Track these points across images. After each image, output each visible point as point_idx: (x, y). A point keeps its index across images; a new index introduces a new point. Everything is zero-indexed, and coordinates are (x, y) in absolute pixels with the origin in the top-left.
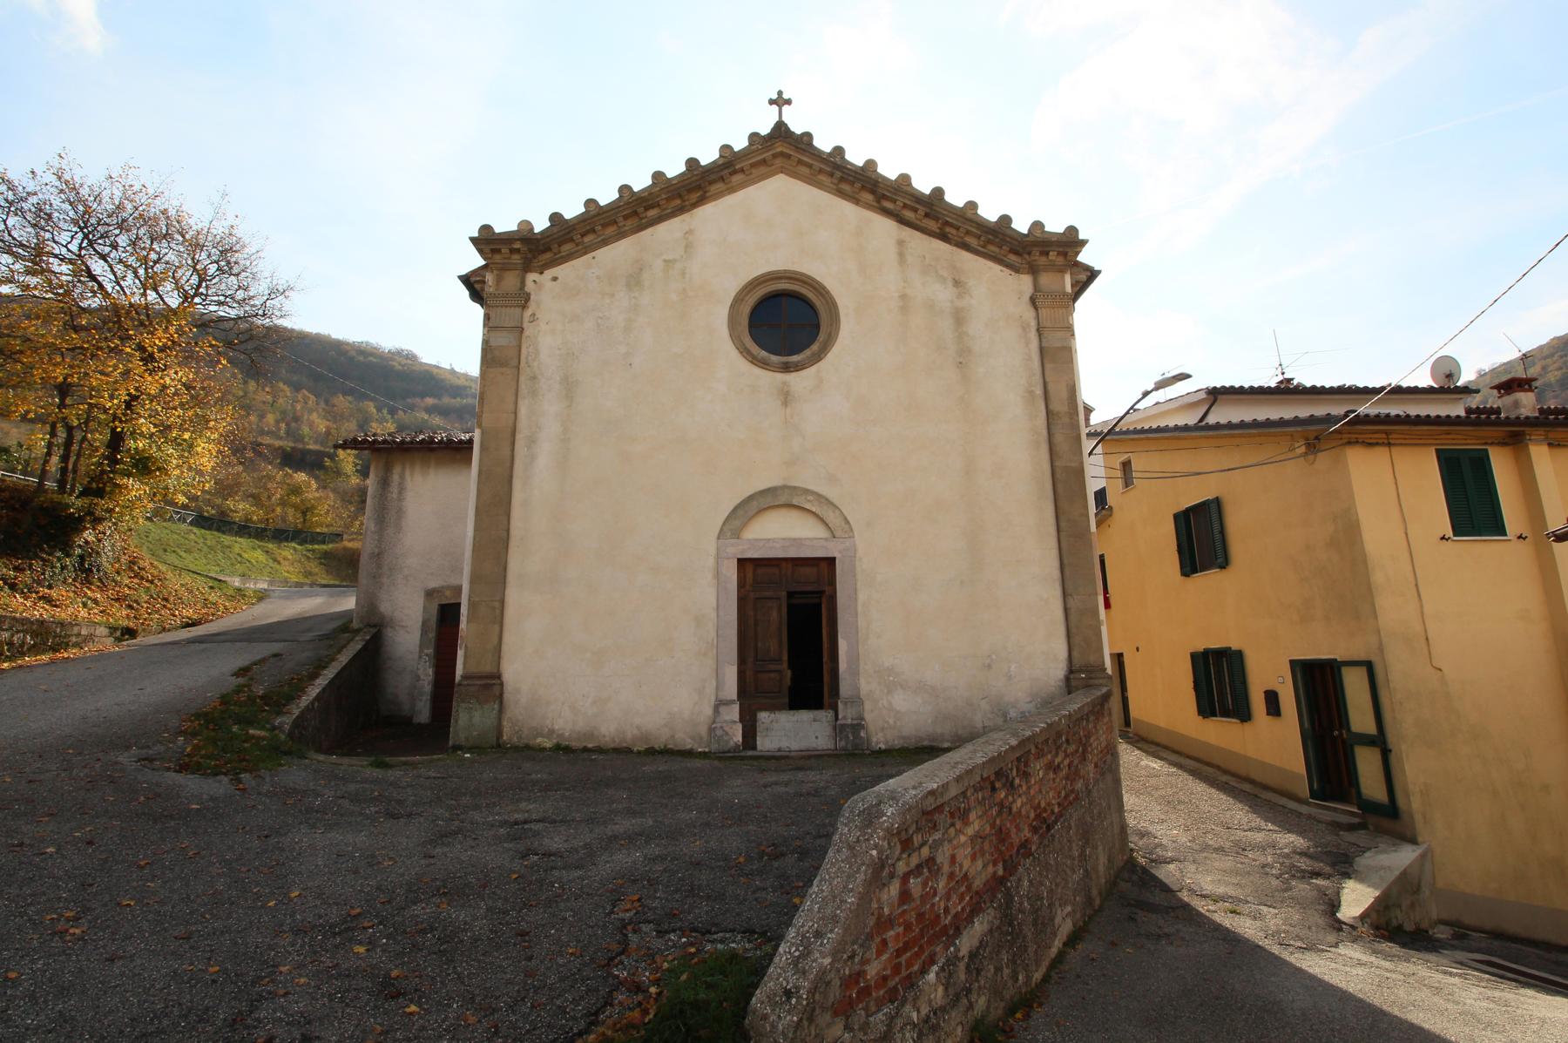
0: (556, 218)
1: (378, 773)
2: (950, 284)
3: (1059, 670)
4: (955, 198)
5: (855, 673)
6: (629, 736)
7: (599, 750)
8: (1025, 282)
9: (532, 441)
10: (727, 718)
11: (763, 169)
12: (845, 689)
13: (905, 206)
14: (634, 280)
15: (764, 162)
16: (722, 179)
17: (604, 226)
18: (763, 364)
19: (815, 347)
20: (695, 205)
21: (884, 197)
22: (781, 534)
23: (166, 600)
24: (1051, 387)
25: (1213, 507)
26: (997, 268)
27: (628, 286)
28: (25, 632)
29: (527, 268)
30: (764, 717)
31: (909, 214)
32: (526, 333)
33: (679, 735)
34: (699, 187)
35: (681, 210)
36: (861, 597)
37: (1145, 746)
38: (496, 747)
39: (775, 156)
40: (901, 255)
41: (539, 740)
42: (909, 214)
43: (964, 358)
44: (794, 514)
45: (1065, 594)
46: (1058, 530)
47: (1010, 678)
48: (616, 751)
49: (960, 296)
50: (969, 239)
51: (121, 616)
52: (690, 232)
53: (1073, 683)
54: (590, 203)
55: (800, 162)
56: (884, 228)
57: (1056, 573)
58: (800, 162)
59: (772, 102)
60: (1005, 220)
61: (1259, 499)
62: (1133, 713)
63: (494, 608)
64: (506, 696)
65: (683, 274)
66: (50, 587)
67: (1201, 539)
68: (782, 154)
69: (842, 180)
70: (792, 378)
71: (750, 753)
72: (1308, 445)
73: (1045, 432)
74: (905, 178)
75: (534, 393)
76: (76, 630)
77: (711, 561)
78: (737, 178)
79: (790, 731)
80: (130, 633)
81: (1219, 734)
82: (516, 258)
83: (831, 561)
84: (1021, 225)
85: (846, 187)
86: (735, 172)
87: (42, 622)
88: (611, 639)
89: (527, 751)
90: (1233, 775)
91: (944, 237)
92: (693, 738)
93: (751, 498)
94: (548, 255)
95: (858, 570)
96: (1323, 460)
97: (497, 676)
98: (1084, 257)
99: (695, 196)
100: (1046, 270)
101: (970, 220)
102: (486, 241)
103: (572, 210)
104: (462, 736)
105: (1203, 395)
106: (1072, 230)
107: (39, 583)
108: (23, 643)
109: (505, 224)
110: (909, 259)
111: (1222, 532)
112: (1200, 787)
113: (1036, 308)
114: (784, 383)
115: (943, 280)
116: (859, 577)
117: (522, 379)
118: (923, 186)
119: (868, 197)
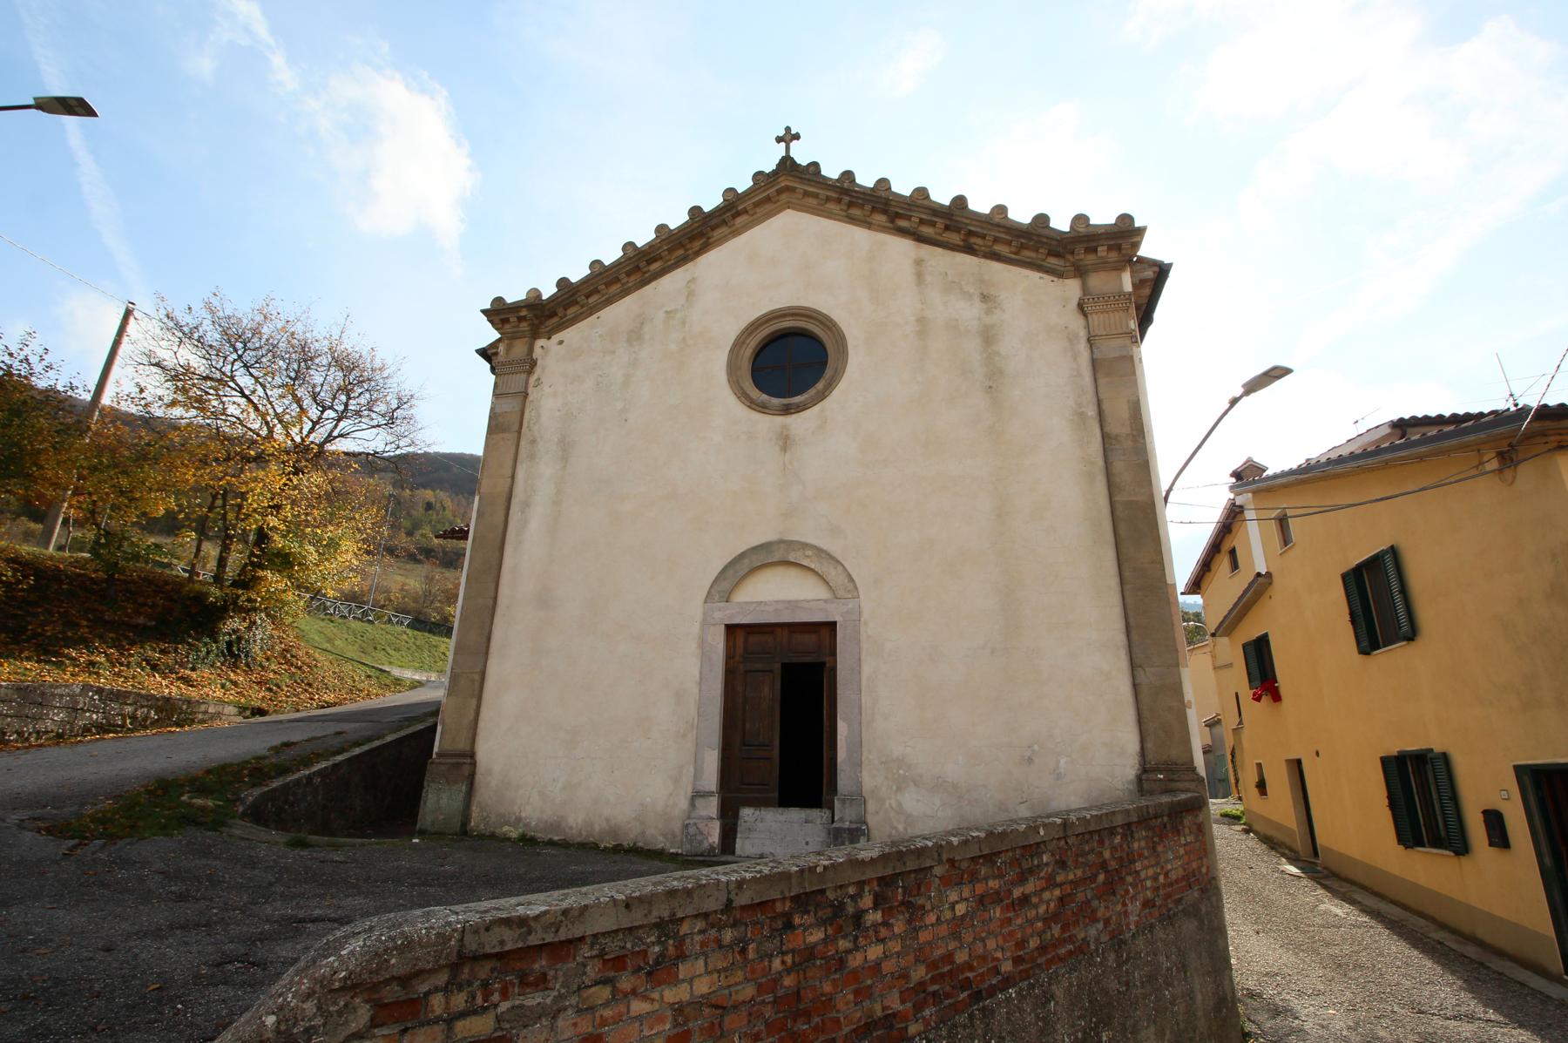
0: (563, 283)
1: (292, 856)
2: (977, 300)
3: (1128, 768)
4: (980, 205)
5: (858, 765)
6: (597, 829)
7: (565, 845)
8: (1072, 288)
9: (526, 505)
10: (704, 813)
11: (768, 207)
12: (844, 782)
13: (922, 221)
14: (635, 335)
15: (768, 199)
16: (724, 223)
17: (608, 285)
18: (762, 408)
19: (820, 385)
20: (698, 253)
21: (898, 216)
22: (777, 595)
23: (310, 685)
24: (1105, 406)
25: (1388, 559)
26: (1034, 276)
27: (629, 341)
28: (150, 707)
29: (535, 335)
30: (747, 813)
31: (927, 231)
32: (530, 398)
33: (650, 831)
34: (702, 234)
35: (685, 260)
36: (866, 670)
37: (1336, 885)
38: (462, 832)
39: (779, 192)
40: (919, 276)
41: (506, 828)
42: (927, 231)
43: (994, 379)
44: (793, 572)
45: (1133, 666)
46: (1122, 582)
47: (1058, 777)
48: (583, 846)
49: (989, 312)
50: (998, 248)
51: (257, 697)
52: (693, 280)
53: (1146, 786)
54: (595, 264)
55: (806, 194)
56: (900, 249)
57: (1120, 638)
58: (806, 194)
59: (779, 140)
60: (1042, 219)
61: (1448, 543)
62: (1319, 841)
63: (473, 681)
64: (478, 777)
65: (684, 323)
66: (193, 669)
67: (1378, 604)
68: (788, 189)
69: (850, 205)
70: (793, 421)
71: (730, 858)
72: (1501, 455)
73: (1100, 462)
74: (922, 192)
75: (532, 457)
76: (203, 707)
77: (696, 629)
78: (740, 220)
79: (780, 838)
80: (261, 712)
81: (1426, 870)
82: (524, 326)
83: (832, 626)
84: (1061, 223)
85: (855, 212)
86: (738, 214)
87: (168, 700)
88: (593, 722)
89: (492, 840)
90: (1454, 931)
91: (969, 250)
92: (665, 836)
93: (742, 556)
94: (555, 320)
95: (863, 637)
96: (1526, 474)
97: (471, 755)
98: (1147, 250)
99: (697, 244)
100: (1096, 270)
101: (998, 225)
102: (498, 313)
103: (578, 272)
104: (429, 819)
105: (1388, 431)
106: (1126, 219)
107: (182, 665)
108: (146, 718)
109: (515, 294)
110: (929, 278)
111: (1404, 590)
112: (1395, 947)
113: (1085, 315)
114: (784, 427)
115: (968, 296)
116: (864, 645)
117: (523, 443)
118: (942, 196)
119: (880, 218)
